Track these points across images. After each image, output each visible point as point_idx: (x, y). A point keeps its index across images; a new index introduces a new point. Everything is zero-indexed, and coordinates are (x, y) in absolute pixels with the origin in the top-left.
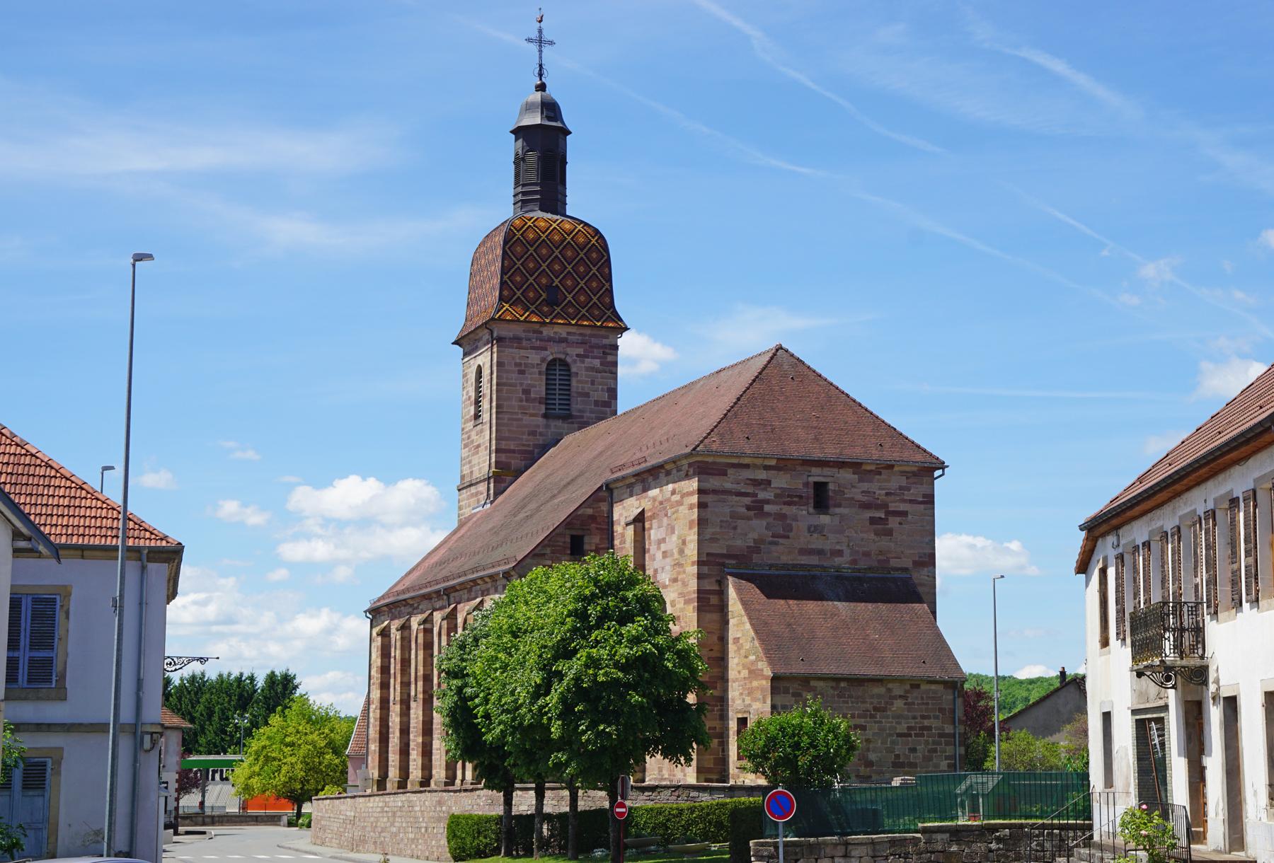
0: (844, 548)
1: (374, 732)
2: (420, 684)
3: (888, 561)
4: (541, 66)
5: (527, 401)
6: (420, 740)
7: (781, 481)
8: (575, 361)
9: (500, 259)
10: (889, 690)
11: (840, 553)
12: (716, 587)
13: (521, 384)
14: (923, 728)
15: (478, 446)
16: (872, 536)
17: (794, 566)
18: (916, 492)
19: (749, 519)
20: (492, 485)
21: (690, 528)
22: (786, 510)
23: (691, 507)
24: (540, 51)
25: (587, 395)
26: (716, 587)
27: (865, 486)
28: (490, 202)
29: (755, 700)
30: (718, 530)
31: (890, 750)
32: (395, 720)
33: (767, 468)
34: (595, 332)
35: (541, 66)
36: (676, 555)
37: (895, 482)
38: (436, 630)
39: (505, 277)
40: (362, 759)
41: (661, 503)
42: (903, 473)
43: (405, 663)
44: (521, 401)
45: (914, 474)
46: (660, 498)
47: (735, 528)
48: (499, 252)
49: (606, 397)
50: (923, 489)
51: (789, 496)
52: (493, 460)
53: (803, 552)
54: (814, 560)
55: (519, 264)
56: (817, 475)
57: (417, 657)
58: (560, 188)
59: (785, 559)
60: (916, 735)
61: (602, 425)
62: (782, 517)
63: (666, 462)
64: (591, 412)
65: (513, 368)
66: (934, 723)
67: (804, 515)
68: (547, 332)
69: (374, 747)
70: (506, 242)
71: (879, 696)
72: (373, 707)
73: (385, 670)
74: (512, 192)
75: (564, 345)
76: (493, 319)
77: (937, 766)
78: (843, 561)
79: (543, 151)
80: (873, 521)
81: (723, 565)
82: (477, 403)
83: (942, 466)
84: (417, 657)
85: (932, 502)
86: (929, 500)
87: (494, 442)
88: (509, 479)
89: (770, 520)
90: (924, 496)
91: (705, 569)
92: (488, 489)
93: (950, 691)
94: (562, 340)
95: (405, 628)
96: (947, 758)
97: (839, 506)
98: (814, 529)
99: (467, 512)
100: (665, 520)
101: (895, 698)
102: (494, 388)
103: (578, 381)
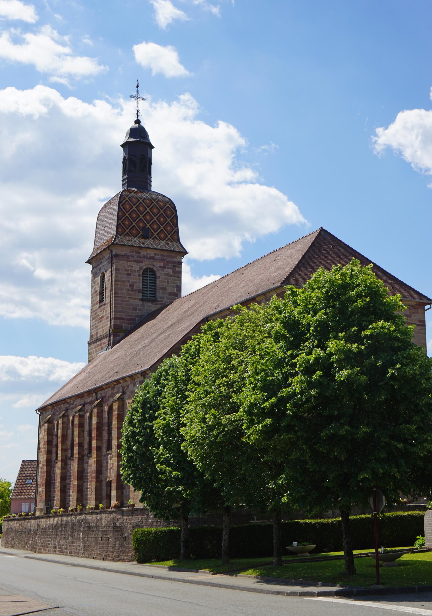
1: (41, 479)
4: (138, 111)
5: (131, 291)
6: (76, 483)
8: (158, 270)
13: (129, 281)
15: (102, 317)
25: (165, 289)
28: (111, 186)
35: (138, 111)
44: (128, 290)
49: (175, 290)
55: (127, 214)
58: (148, 176)
61: (176, 303)
64: (167, 299)
65: (124, 272)
73: (102, 293)
74: (121, 178)
75: (152, 260)
76: (113, 244)
79: (138, 151)
85: (424, 325)
88: (122, 335)
90: (420, 321)
103: (160, 281)
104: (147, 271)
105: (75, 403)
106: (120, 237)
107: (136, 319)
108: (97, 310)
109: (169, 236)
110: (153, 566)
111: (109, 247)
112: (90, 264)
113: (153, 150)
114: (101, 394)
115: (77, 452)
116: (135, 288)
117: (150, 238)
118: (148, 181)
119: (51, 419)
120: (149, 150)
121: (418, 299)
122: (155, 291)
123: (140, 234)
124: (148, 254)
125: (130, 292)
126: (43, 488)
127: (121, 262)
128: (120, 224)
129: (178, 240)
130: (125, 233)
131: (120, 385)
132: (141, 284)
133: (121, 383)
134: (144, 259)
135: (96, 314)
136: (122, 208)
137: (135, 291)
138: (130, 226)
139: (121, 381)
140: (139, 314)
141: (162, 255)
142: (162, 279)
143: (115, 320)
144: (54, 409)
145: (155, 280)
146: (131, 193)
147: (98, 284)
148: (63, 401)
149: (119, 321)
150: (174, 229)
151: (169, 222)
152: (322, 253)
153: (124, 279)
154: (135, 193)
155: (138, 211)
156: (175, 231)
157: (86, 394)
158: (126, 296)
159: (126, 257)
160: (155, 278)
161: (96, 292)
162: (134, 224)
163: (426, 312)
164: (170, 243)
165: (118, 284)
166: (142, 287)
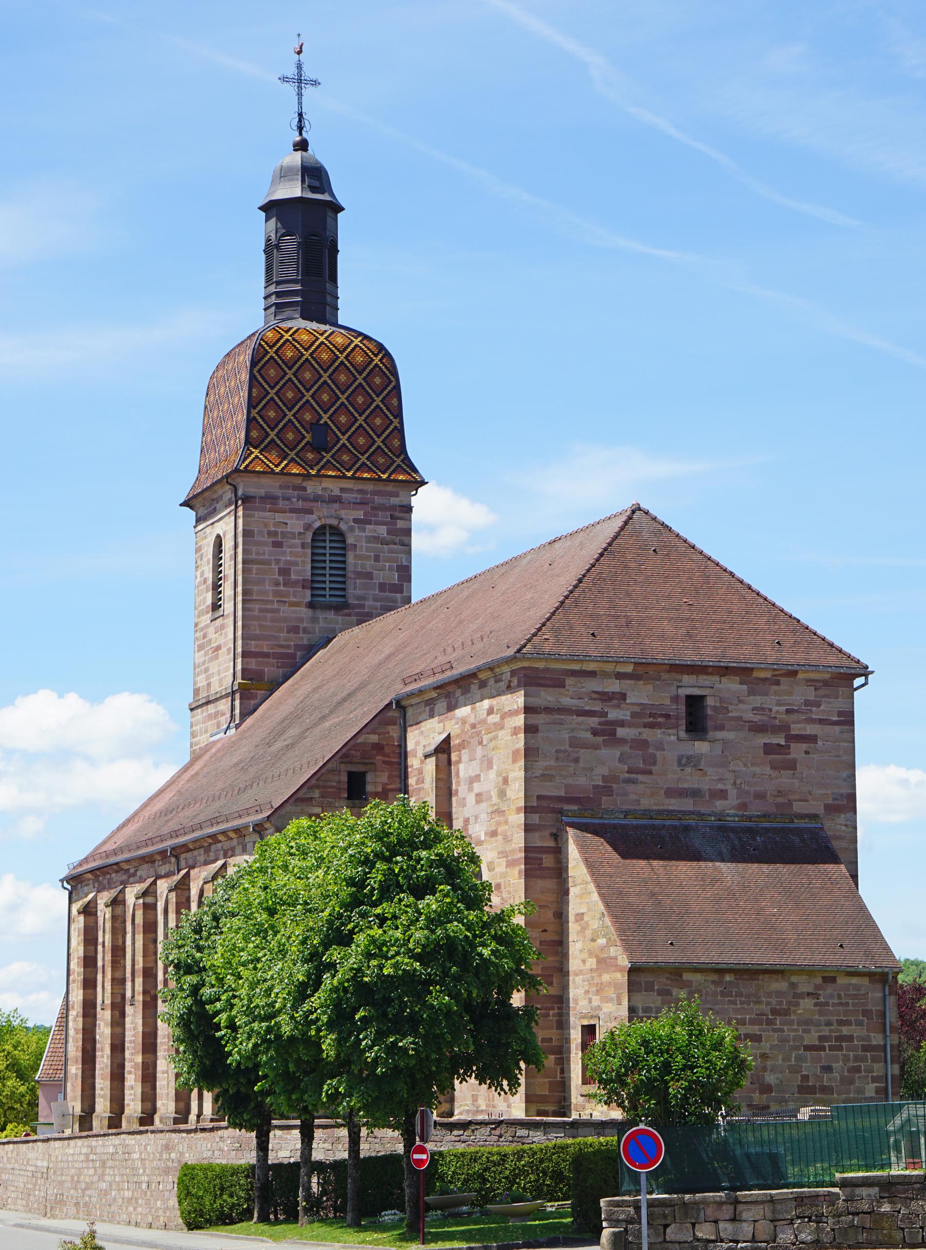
0: (729, 787)
1: (74, 1049)
2: (139, 981)
3: (790, 804)
4: (300, 115)
5: (285, 585)
7: (640, 694)
8: (352, 529)
9: (246, 387)
10: (793, 986)
11: (723, 794)
12: (551, 843)
13: (278, 561)
14: (841, 1038)
15: (218, 648)
16: (768, 770)
17: (660, 812)
18: (829, 708)
19: (596, 747)
20: (237, 703)
21: (514, 761)
22: (647, 734)
23: (515, 732)
24: (300, 95)
26: (551, 843)
27: (757, 701)
28: (237, 306)
29: (607, 1000)
31: (795, 1070)
32: (104, 1032)
33: (620, 676)
34: (380, 487)
35: (300, 115)
36: (495, 799)
37: (800, 694)
38: (160, 906)
39: (254, 413)
40: (58, 1086)
41: (473, 726)
42: (810, 682)
43: (118, 951)
45: (826, 683)
46: (472, 720)
47: (576, 760)
48: (245, 376)
51: (651, 715)
52: (239, 667)
53: (671, 793)
54: (687, 804)
55: (272, 393)
56: (691, 685)
57: (134, 943)
58: (328, 286)
59: (647, 803)
62: (644, 744)
63: (479, 669)
64: (376, 599)
67: (672, 742)
68: (312, 487)
69: (75, 1069)
70: (254, 363)
71: (779, 994)
72: (73, 1013)
73: (89, 962)
75: (336, 506)
76: (237, 470)
77: (860, 1091)
78: (727, 806)
80: (769, 749)
81: (561, 812)
82: (216, 587)
83: (865, 672)
84: (134, 943)
85: (852, 723)
86: (847, 719)
87: (239, 642)
89: (626, 749)
90: (840, 714)
91: (536, 819)
92: (233, 709)
93: (879, 986)
95: (117, 902)
96: (874, 1080)
97: (721, 728)
99: (203, 740)
100: (479, 751)
101: (801, 996)
102: (240, 566)
104: (325, 534)
105: (139, 874)
107: (298, 653)
108: (207, 626)
110: (207, 1235)
111: (227, 476)
112: (191, 508)
114: (186, 859)
115: (141, 989)
116: (293, 577)
119: (91, 905)
120: (329, 220)
122: (344, 582)
124: (324, 489)
125: (282, 588)
126: (77, 1069)
128: (254, 418)
131: (219, 845)
133: (220, 841)
134: (315, 504)
135: (204, 636)
136: (258, 377)
137: (295, 583)
138: (280, 421)
139: (221, 838)
140: (305, 642)
142: (361, 550)
144: (98, 881)
145: (344, 555)
147: (208, 561)
148: (115, 867)
149: (254, 660)
151: (378, 406)
153: (267, 557)
156: (395, 427)
157: (158, 857)
160: (344, 549)
161: (205, 581)
162: (290, 415)
163: (855, 693)
165: (250, 570)
166: (312, 574)
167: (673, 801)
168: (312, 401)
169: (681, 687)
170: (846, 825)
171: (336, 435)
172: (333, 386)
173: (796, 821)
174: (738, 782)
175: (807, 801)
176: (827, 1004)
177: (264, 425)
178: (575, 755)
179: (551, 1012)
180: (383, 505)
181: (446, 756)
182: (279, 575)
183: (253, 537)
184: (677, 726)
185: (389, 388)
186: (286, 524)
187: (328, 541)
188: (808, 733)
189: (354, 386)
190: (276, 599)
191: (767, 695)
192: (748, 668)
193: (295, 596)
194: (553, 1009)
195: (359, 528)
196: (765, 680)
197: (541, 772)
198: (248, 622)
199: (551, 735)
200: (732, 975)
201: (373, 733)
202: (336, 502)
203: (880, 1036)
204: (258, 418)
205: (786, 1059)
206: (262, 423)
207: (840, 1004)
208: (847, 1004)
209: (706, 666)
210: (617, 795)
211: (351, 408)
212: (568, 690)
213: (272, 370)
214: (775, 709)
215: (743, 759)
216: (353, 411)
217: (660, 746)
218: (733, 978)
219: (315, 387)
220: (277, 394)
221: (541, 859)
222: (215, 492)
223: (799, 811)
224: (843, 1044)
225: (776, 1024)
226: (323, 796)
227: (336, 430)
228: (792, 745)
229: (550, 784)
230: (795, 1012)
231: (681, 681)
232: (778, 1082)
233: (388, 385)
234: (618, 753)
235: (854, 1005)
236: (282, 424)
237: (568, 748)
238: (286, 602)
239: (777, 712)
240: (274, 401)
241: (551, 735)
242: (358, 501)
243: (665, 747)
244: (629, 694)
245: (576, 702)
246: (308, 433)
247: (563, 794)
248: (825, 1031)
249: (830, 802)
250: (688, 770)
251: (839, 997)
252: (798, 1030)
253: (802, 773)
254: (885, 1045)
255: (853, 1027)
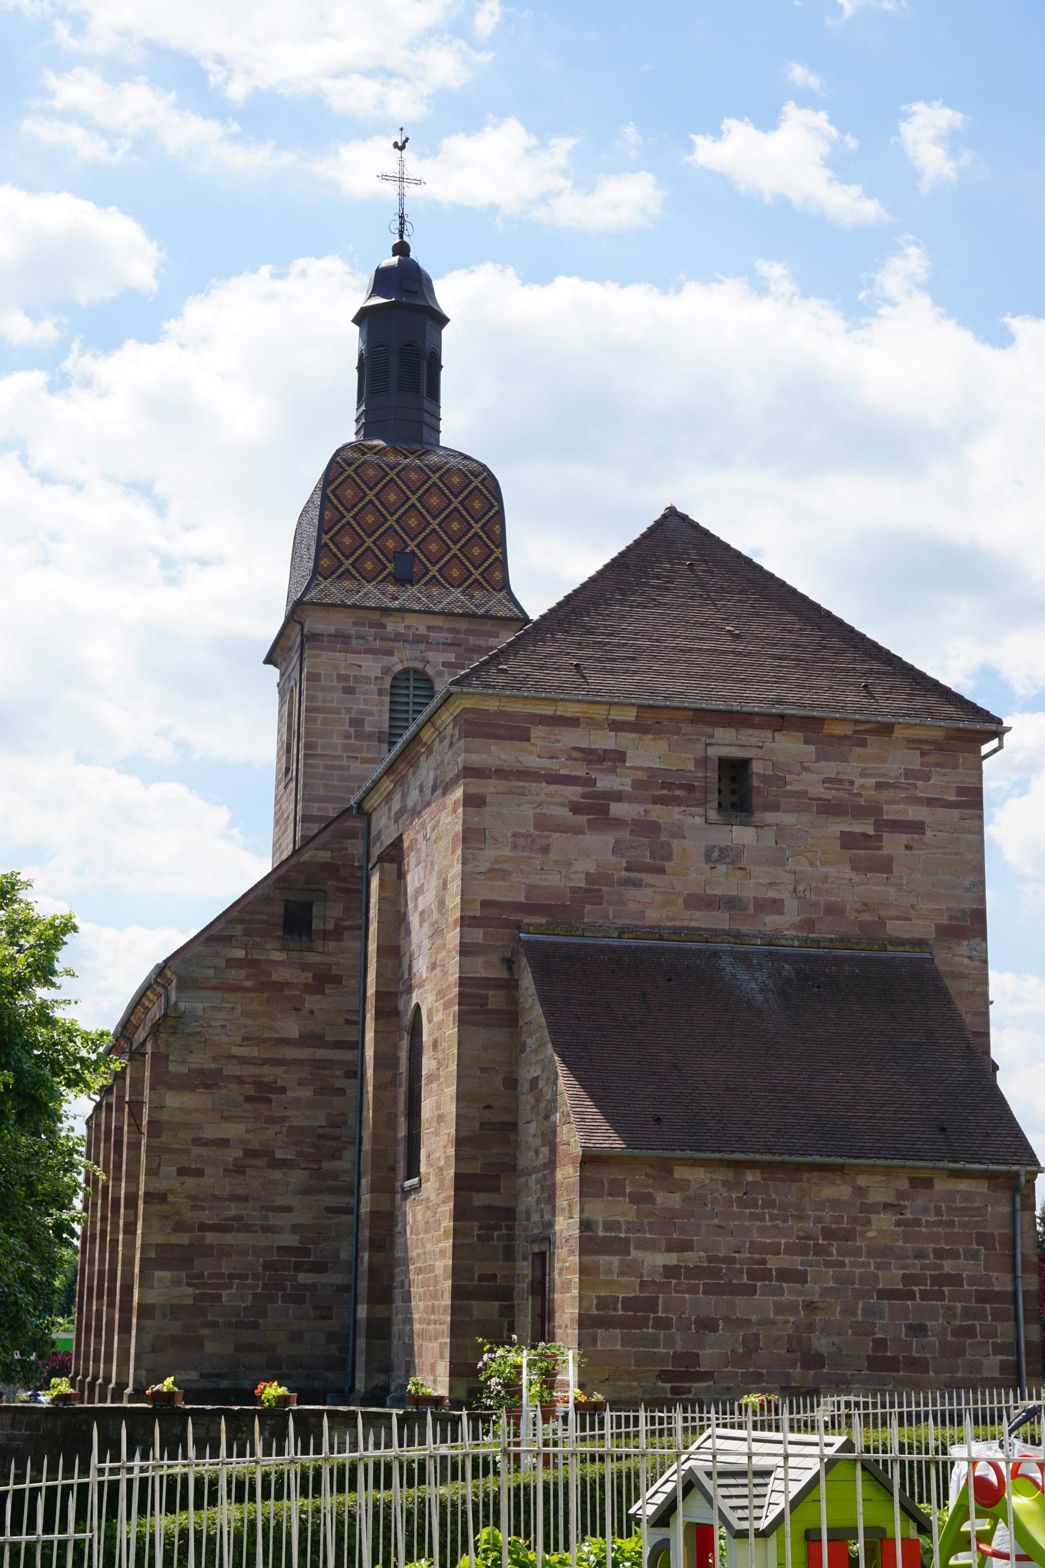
0: (785, 895)
3: (881, 922)
4: (402, 217)
5: (357, 737)
7: (648, 754)
8: (440, 674)
10: (861, 1192)
11: (776, 906)
12: (501, 973)
13: (349, 710)
14: (940, 1280)
16: (847, 872)
17: (677, 931)
18: (942, 782)
19: (577, 831)
22: (657, 813)
26: (501, 973)
27: (831, 768)
30: (507, 852)
31: (863, 1330)
33: (617, 726)
35: (402, 217)
36: (435, 915)
39: (325, 538)
42: (913, 743)
44: (347, 736)
45: (938, 746)
47: (545, 850)
50: (959, 777)
51: (664, 785)
53: (693, 901)
54: (720, 920)
55: (349, 516)
56: (727, 743)
58: (427, 404)
59: (654, 916)
60: (924, 1296)
66: (967, 1268)
67: (696, 829)
71: (836, 1204)
75: (422, 646)
77: (974, 1367)
78: (784, 923)
79: (400, 336)
80: (848, 841)
81: (518, 926)
86: (971, 799)
89: (624, 834)
90: (960, 791)
91: (478, 935)
93: (1004, 1195)
94: (419, 640)
96: (998, 1349)
97: (776, 808)
98: (717, 856)
101: (874, 1208)
104: (408, 679)
106: (325, 584)
109: (347, 564)
113: (446, 332)
116: (367, 729)
117: (418, 581)
118: (427, 417)
121: (951, 719)
123: (386, 572)
124: (408, 627)
125: (353, 741)
127: (326, 655)
128: (326, 544)
129: (504, 585)
130: (339, 572)
132: (386, 717)
134: (396, 644)
136: (332, 497)
137: (369, 736)
138: (357, 549)
141: (451, 630)
143: (306, 825)
146: (364, 454)
150: (492, 552)
151: (476, 534)
152: (646, 584)
153: (335, 705)
154: (375, 454)
155: (382, 503)
158: (339, 753)
159: (341, 640)
162: (369, 542)
163: (985, 763)
164: (477, 594)
165: (315, 720)
167: (697, 914)
168: (396, 526)
169: (711, 744)
170: (970, 958)
171: (425, 565)
172: (423, 510)
173: (889, 948)
174: (800, 888)
175: (910, 919)
176: (917, 1223)
177: (338, 553)
178: (544, 842)
179: (496, 1234)
180: (479, 646)
181: (395, 865)
182: (350, 726)
183: (319, 681)
184: (706, 803)
185: (491, 514)
186: (360, 666)
187: (411, 688)
188: (910, 818)
189: (449, 510)
190: (345, 754)
191: (847, 761)
192: (814, 718)
193: (368, 750)
194: (500, 1229)
195: (449, 673)
196: (843, 738)
197: (488, 865)
198: (311, 781)
199: (505, 811)
200: (758, 1172)
201: (324, 848)
202: (422, 642)
203: (1008, 1277)
204: (331, 544)
205: (848, 1311)
206: (335, 550)
207: (940, 1223)
208: (951, 1224)
209: (750, 714)
210: (609, 903)
211: (443, 535)
212: (534, 745)
213: (349, 491)
214: (859, 781)
215: (808, 855)
216: (446, 538)
217: (678, 833)
218: (758, 1179)
219: (401, 511)
220: (354, 518)
221: (486, 997)
222: (289, 638)
223: (894, 934)
224: (946, 1289)
225: (830, 1254)
226: (248, 933)
227: (424, 560)
228: (885, 835)
229: (502, 883)
230: (862, 1235)
231: (712, 736)
232: (834, 1349)
233: (489, 510)
234: (611, 841)
235: (963, 1225)
236: (359, 552)
237: (532, 831)
238: (357, 758)
239: (862, 786)
240: (351, 525)
241: (505, 811)
242: (449, 641)
243: (686, 833)
244: (629, 753)
245: (546, 763)
246: (390, 562)
247: (523, 900)
248: (914, 1266)
249: (945, 921)
250: (722, 868)
251: (938, 1211)
252: (868, 1265)
253: (901, 878)
254: (1015, 1293)
255: (962, 1261)
